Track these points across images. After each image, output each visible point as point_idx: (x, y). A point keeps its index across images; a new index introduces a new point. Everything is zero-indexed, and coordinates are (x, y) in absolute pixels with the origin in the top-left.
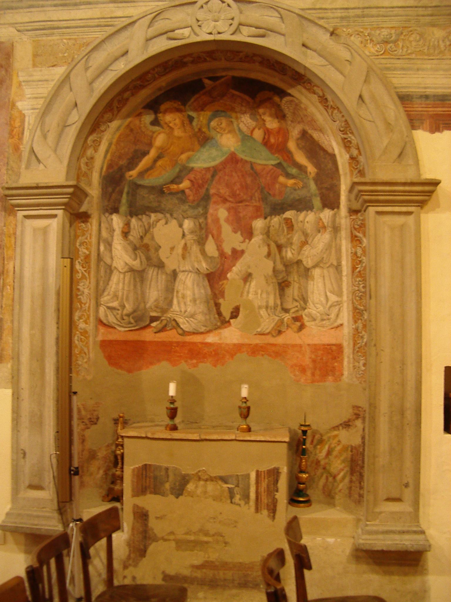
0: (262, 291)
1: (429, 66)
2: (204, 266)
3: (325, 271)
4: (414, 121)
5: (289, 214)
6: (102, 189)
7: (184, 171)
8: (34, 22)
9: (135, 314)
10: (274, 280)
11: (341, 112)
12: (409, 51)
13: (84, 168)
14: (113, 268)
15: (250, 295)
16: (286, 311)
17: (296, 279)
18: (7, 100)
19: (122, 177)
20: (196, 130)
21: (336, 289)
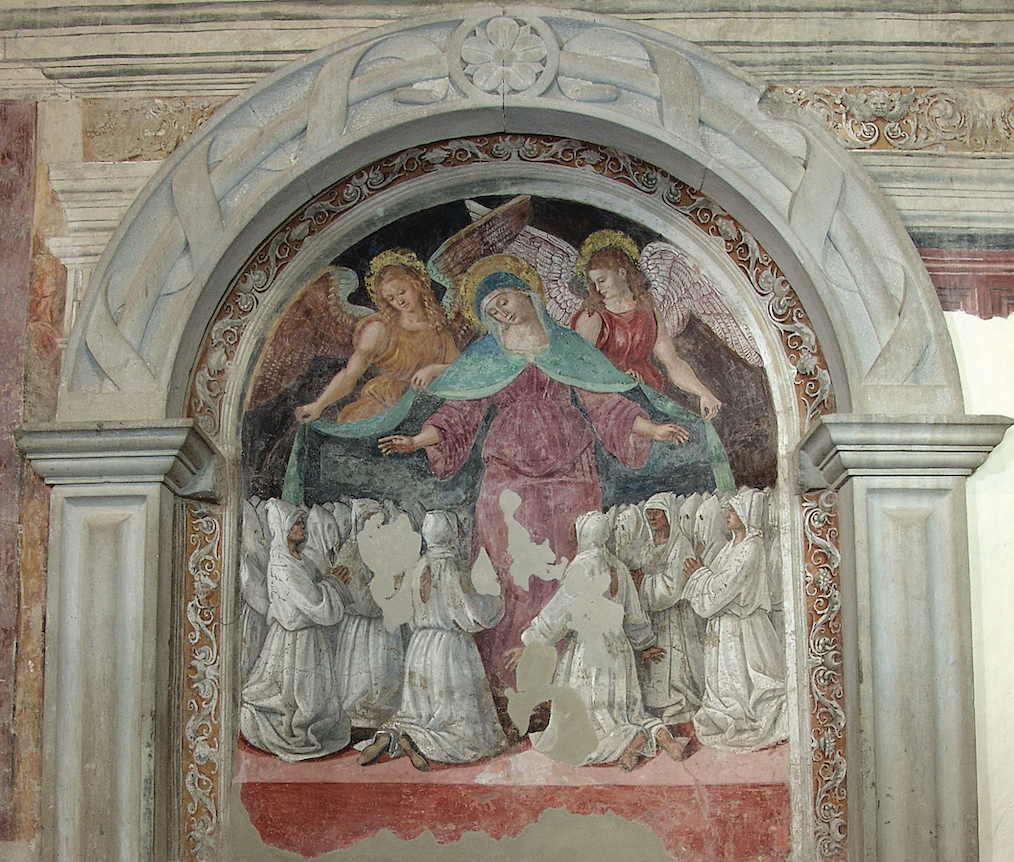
0: (599, 670)
1: (975, 173)
2: (469, 616)
3: (744, 624)
4: (947, 292)
5: (657, 501)
6: (244, 445)
7: (426, 407)
8: (85, 57)
9: (319, 723)
10: (627, 646)
11: (779, 273)
12: (931, 140)
13: (203, 394)
14: (269, 622)
15: (573, 680)
16: (656, 712)
17: (676, 642)
18: (23, 234)
19: (288, 416)
20: (451, 316)
21: (770, 662)
